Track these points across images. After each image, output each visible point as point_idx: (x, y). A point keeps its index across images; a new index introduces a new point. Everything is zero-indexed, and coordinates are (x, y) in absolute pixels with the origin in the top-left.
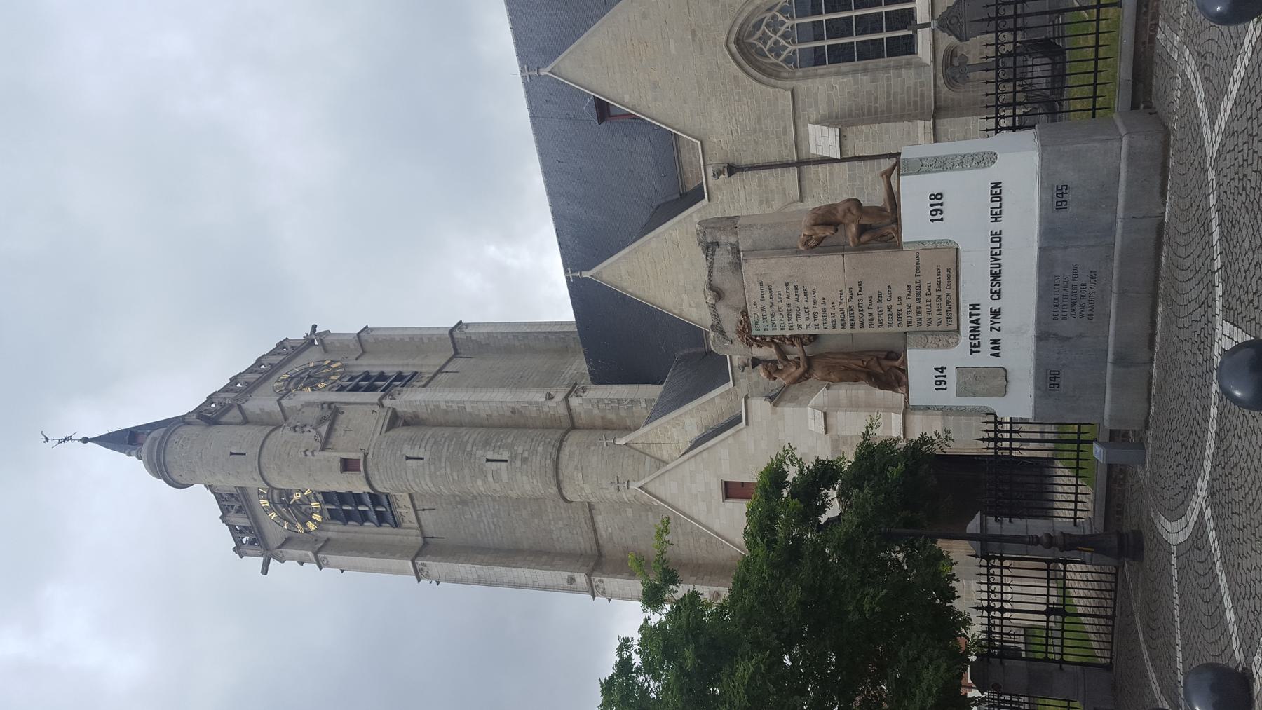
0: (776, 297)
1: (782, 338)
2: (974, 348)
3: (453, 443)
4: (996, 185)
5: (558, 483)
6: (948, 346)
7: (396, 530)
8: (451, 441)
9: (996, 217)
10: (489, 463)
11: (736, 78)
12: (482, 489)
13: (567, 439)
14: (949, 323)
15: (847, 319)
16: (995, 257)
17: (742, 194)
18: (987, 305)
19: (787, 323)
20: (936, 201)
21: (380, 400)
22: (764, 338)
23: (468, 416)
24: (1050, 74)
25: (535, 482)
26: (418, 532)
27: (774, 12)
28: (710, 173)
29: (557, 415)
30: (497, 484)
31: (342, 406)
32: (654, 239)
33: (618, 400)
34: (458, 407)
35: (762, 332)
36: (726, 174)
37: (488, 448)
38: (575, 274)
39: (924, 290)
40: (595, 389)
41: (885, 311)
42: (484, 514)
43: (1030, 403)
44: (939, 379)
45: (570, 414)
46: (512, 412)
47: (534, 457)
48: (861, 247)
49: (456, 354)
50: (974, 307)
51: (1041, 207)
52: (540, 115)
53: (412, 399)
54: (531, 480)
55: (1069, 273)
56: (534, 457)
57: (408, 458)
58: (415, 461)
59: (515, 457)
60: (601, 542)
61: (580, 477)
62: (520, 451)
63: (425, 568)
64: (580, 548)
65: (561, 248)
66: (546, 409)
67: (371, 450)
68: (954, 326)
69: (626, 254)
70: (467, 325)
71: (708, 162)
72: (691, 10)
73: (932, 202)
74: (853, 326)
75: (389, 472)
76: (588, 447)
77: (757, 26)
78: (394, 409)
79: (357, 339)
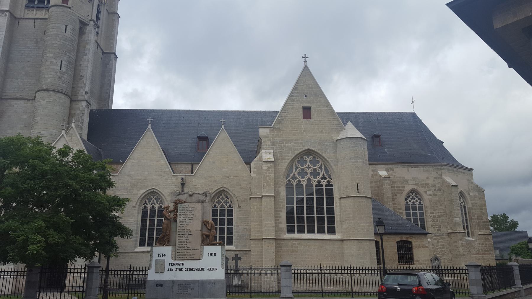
0: (190, 211)
1: (177, 212)
2: (171, 264)
3: (72, 48)
4: (216, 269)
5: (48, 90)
6: (172, 257)
7: (24, 6)
8: (72, 47)
9: (208, 269)
10: (60, 62)
11: (212, 189)
12: (48, 55)
13: (67, 98)
14: (177, 258)
15: (181, 231)
16: (197, 269)
17: (174, 187)
18: (183, 267)
19: (182, 214)
20: (214, 254)
21: (93, 20)
22: (177, 207)
23: (81, 56)
24: (60, 294)
25: (49, 80)
26: (22, 17)
27: (230, 203)
28: (183, 177)
29: (78, 95)
30: (49, 63)
31: (92, 2)
32: (161, 154)
33: (83, 122)
34: (86, 53)
35: (179, 207)
36: (182, 182)
37: (67, 62)
38: (150, 122)
39: (188, 251)
40: (88, 113)
41: (183, 241)
42: (29, 50)
43: (152, 279)
44: (162, 255)
45: (78, 101)
46: (81, 75)
47: (62, 82)
48: (202, 235)
49: (104, 53)
50: (183, 264)
51: (210, 280)
52: (200, 114)
53: (92, 34)
54: (51, 78)
55: (191, 288)
56: (62, 82)
57: (66, 26)
58: (65, 29)
59: (62, 74)
60: (9, 100)
61: (50, 101)
62: (65, 76)
63: (3, 15)
64: (6, 90)
65: (149, 110)
66: (82, 90)
67: (72, 11)
68: (177, 259)
69: (156, 142)
70: (116, 60)
71: (186, 176)
72: (234, 177)
73: (214, 254)
74: (179, 232)
75: (61, 16)
76: (63, 106)
77: (227, 197)
78: (88, 25)
79: (115, 12)
